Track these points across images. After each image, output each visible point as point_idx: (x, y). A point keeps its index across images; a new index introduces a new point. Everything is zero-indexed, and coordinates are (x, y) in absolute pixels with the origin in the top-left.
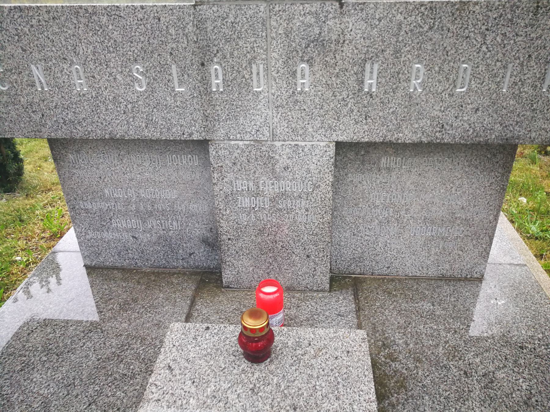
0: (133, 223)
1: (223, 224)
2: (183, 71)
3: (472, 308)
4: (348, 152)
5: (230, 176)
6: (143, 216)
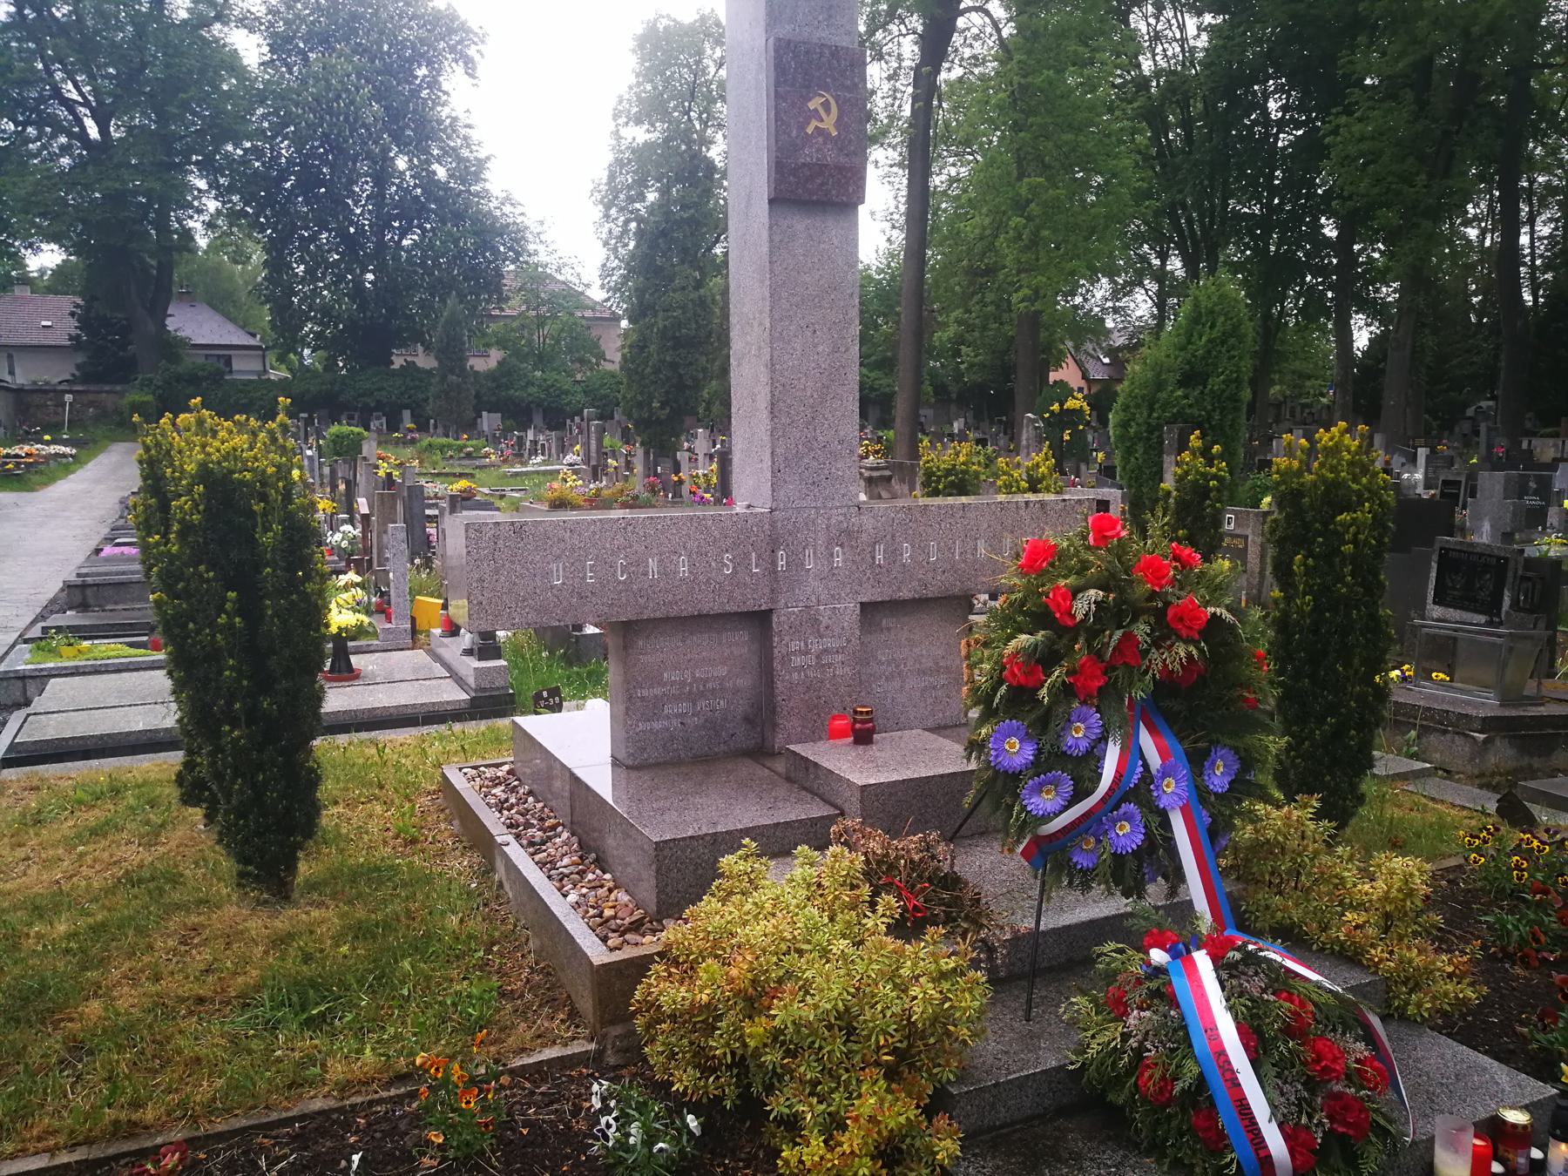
0: (684, 707)
1: (779, 684)
2: (759, 557)
3: (755, 1030)
4: (869, 610)
5: (787, 638)
6: (693, 698)
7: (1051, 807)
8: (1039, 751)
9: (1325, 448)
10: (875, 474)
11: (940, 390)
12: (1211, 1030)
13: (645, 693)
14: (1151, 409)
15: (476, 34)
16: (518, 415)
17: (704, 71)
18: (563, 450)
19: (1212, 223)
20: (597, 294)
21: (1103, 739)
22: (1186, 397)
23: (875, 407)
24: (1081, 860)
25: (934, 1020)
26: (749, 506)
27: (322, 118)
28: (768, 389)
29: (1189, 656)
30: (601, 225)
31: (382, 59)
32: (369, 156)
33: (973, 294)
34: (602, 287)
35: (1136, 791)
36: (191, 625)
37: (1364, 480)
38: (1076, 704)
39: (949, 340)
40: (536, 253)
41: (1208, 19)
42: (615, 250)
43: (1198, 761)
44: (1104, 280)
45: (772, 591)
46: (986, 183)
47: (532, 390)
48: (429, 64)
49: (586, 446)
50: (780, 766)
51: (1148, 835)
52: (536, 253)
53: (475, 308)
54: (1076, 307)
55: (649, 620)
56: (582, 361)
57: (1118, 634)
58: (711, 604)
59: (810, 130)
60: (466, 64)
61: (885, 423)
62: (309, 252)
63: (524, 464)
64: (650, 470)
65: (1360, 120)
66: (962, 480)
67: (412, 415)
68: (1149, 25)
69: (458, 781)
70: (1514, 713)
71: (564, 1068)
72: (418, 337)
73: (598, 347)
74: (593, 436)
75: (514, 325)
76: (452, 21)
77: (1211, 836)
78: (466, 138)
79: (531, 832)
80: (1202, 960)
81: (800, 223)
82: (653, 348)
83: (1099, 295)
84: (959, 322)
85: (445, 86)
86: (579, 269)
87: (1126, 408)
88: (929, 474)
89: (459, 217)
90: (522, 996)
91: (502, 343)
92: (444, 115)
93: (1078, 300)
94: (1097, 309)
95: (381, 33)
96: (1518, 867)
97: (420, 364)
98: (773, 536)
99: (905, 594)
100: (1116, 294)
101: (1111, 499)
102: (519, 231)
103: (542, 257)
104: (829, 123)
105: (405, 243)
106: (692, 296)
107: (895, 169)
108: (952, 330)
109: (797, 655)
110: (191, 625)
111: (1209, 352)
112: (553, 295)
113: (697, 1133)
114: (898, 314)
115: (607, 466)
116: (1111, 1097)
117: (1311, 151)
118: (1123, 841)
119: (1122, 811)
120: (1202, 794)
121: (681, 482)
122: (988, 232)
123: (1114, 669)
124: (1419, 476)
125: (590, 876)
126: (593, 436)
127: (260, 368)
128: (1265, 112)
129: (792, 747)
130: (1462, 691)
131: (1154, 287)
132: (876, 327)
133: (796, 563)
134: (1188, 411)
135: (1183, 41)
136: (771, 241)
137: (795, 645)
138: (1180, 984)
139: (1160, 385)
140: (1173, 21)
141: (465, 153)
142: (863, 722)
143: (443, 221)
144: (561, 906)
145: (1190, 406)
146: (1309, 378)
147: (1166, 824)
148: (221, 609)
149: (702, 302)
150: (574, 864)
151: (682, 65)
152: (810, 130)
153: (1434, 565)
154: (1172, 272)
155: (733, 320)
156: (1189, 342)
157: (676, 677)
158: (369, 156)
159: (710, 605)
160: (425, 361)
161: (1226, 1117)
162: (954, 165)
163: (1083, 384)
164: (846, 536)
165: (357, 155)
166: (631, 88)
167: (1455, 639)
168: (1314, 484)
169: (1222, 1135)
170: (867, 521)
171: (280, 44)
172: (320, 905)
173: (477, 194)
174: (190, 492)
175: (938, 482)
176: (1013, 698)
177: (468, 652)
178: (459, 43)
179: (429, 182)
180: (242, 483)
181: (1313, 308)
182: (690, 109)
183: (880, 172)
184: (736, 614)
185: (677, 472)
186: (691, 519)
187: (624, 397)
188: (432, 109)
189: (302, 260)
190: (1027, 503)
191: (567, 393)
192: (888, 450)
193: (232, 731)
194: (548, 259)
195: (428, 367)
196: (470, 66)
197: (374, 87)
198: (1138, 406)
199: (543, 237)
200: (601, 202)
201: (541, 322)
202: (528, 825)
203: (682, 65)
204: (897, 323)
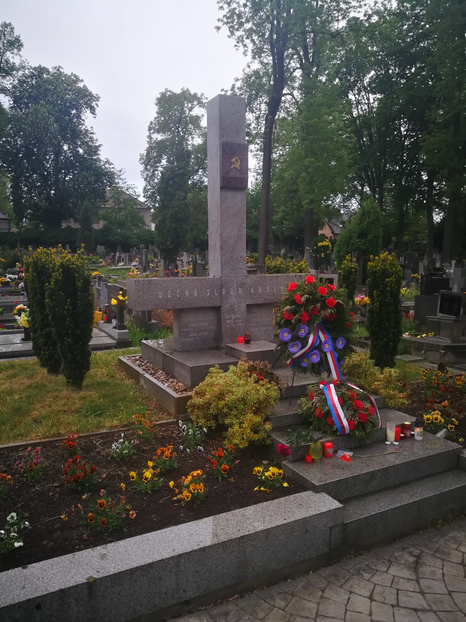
0: (195, 334)
2: (217, 291)
4: (250, 307)
7: (296, 351)
8: (293, 336)
9: (382, 259)
10: (251, 269)
11: (276, 238)
12: (332, 399)
13: (184, 330)
14: (348, 246)
15: (95, 97)
16: (112, 247)
17: (184, 113)
18: (131, 260)
19: (380, 174)
20: (142, 199)
21: (309, 334)
22: (360, 242)
23: (252, 244)
24: (304, 365)
25: (265, 399)
26: (214, 276)
27: (34, 130)
28: (220, 242)
29: (331, 312)
30: (144, 172)
31: (58, 107)
32: (53, 145)
33: (289, 201)
34: (144, 196)
35: (317, 347)
36: (57, 309)
37: (394, 269)
38: (302, 324)
39: (279, 218)
40: (118, 183)
41: (379, 96)
42: (149, 182)
43: (334, 340)
44: (339, 195)
45: (221, 301)
46: (292, 160)
47: (117, 237)
48: (76, 109)
49: (141, 260)
50: (224, 351)
51: (321, 359)
52: (118, 183)
53: (95, 205)
54: (329, 205)
55: (186, 309)
56: (136, 226)
57: (312, 306)
58: (203, 304)
59: (232, 167)
60: (91, 109)
61: (255, 250)
62: (29, 182)
63: (116, 266)
64: (166, 268)
65: (434, 136)
66: (279, 270)
67: (70, 247)
68: (356, 98)
69: (125, 360)
70: (454, 344)
71: (168, 425)
72: (72, 215)
73: (143, 220)
74: (144, 255)
75: (110, 211)
76: (86, 92)
77: (339, 360)
78: (91, 138)
79: (150, 371)
80: (332, 386)
81: (229, 194)
82: (168, 222)
83: (338, 201)
84: (283, 212)
85: (83, 117)
86: (135, 190)
87: (339, 246)
88: (268, 268)
89: (88, 169)
90: (153, 410)
91: (105, 218)
92: (82, 129)
93: (330, 202)
94: (337, 206)
95: (58, 96)
96: (434, 380)
97: (73, 227)
98: (221, 284)
99: (260, 302)
100: (344, 200)
101: (334, 278)
102: (112, 174)
103: (121, 185)
104: (237, 165)
105: (67, 178)
106: (182, 202)
107: (259, 152)
108: (280, 215)
109: (228, 319)
110: (57, 309)
111: (368, 226)
112: (125, 200)
113: (206, 432)
114: (260, 208)
115: (149, 266)
116: (309, 420)
117: (416, 147)
118: (314, 360)
119: (314, 352)
120: (336, 349)
121: (178, 272)
122: (294, 177)
123: (312, 315)
124: (452, 271)
125: (170, 380)
126: (144, 255)
127: (8, 227)
128: (400, 132)
129: (227, 345)
130: (441, 339)
131: (359, 198)
132: (251, 213)
133: (228, 293)
134: (361, 247)
135: (369, 104)
136: (221, 199)
137: (227, 317)
138: (326, 392)
139: (351, 238)
140: (365, 97)
141: (90, 144)
142: (247, 337)
143: (82, 171)
144: (164, 386)
145: (362, 245)
146: (419, 233)
147: (326, 356)
148: (66, 304)
149: (186, 205)
150: (165, 378)
151: (175, 110)
152: (232, 167)
153: (439, 300)
154: (366, 192)
155: (209, 221)
156: (361, 223)
157: (193, 325)
158: (53, 145)
159: (203, 304)
160: (74, 225)
161: (334, 418)
162: (281, 150)
163: (332, 235)
164: (242, 285)
165: (48, 144)
166: (155, 118)
167: (440, 322)
168: (379, 270)
169: (333, 422)
170: (248, 280)
171: (17, 100)
172: (91, 391)
173: (95, 160)
174: (58, 270)
175: (271, 270)
176: (286, 323)
177: (115, 328)
178: (89, 100)
179: (76, 154)
180: (72, 268)
181: (418, 206)
182: (179, 127)
183: (253, 154)
184: (211, 307)
185: (177, 268)
186: (198, 279)
187: (156, 240)
188: (78, 126)
189: (25, 185)
190: (296, 276)
191: (130, 238)
192: (256, 261)
193: (67, 339)
194: (123, 186)
195: (76, 228)
196: (93, 111)
197: (55, 118)
198: (343, 245)
199: (121, 177)
200: (144, 163)
201: (120, 210)
202: (149, 370)
203: (175, 110)
204: (259, 211)
